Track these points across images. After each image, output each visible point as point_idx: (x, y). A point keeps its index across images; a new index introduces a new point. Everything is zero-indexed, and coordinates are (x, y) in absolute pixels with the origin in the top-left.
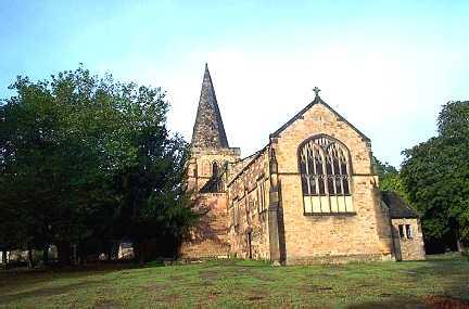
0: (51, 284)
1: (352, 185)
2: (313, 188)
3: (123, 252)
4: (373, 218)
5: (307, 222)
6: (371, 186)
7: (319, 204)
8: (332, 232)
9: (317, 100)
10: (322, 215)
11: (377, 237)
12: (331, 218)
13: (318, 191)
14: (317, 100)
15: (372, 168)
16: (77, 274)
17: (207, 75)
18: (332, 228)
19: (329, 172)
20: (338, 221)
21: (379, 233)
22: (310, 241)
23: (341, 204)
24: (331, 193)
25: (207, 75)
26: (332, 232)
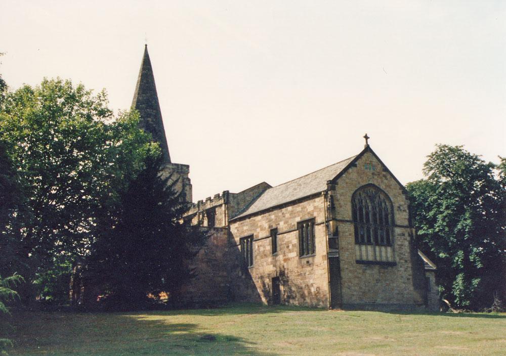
0: (140, 316)
1: (393, 236)
2: (362, 237)
3: (168, 293)
4: (409, 269)
5: (359, 269)
6: (408, 238)
7: (367, 252)
8: (378, 281)
9: (368, 149)
10: (368, 264)
11: (412, 288)
12: (377, 267)
13: (385, 243)
14: (368, 149)
15: (410, 220)
16: (183, 311)
17: (147, 63)
18: (377, 276)
19: (375, 221)
20: (382, 271)
21: (414, 285)
22: (361, 288)
23: (385, 254)
24: (377, 244)
25: (147, 63)
26: (378, 281)
